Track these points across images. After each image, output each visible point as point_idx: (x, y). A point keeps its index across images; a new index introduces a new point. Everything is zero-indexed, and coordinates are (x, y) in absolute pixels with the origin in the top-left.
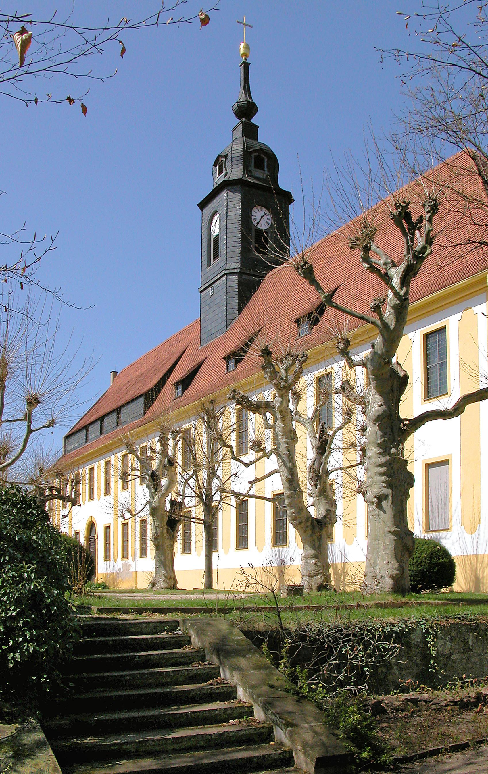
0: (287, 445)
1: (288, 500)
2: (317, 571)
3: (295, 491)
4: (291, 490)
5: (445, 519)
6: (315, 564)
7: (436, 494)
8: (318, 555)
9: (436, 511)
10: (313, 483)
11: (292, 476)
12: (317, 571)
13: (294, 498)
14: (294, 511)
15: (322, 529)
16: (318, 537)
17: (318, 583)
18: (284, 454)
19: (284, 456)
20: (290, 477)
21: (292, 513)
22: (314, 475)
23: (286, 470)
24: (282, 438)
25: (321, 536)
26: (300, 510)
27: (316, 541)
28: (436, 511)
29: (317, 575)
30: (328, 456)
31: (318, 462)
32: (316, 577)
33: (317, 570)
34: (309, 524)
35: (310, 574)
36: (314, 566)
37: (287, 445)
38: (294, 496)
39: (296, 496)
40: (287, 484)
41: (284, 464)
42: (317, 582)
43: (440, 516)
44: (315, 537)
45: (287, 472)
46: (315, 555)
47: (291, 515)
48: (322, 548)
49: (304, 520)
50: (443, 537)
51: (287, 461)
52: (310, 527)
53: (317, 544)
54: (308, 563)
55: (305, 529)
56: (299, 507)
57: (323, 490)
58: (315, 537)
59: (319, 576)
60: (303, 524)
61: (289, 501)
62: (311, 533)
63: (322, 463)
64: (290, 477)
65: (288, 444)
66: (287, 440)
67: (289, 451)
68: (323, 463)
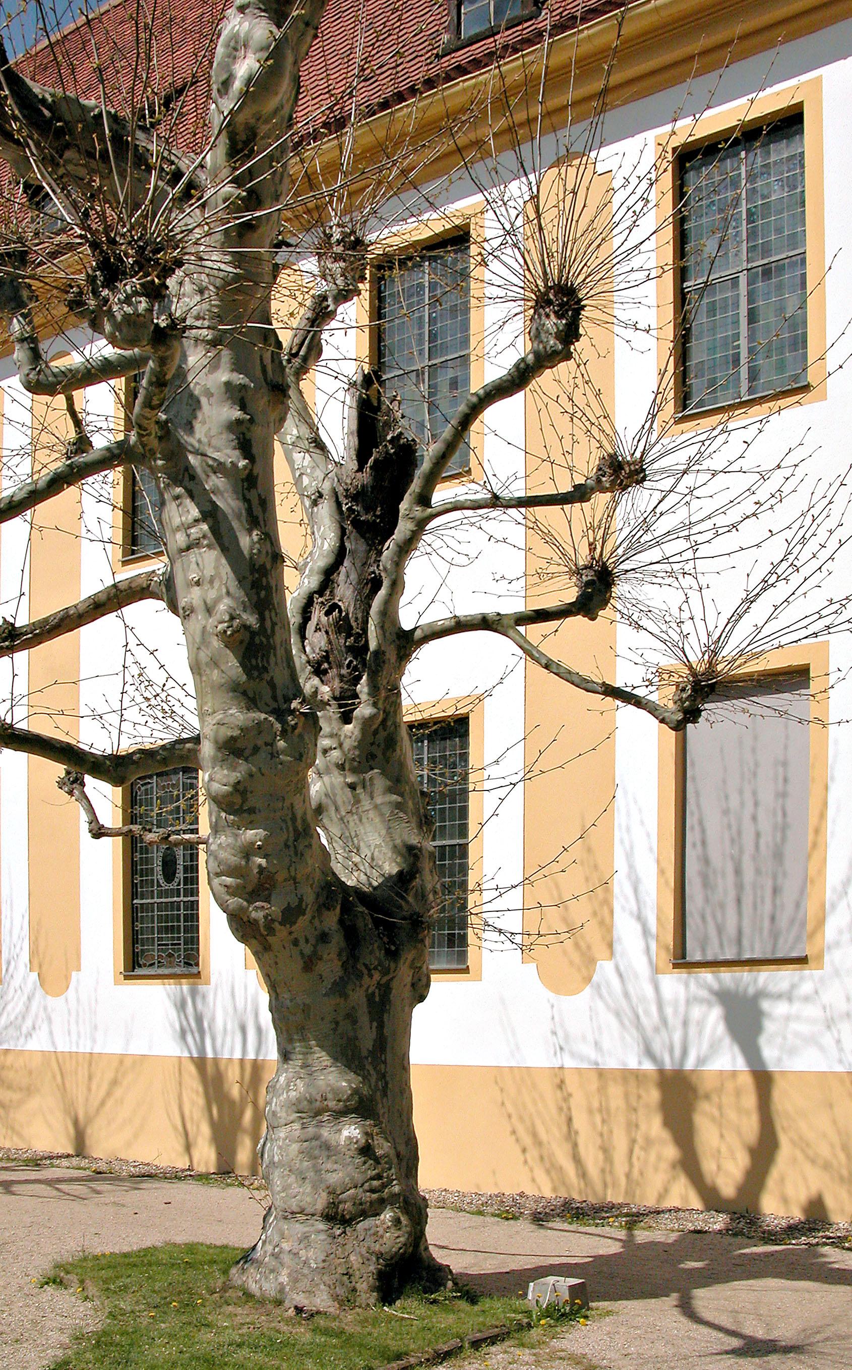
0: (237, 414)
1: (233, 768)
2: (372, 1191)
3: (281, 714)
4: (251, 700)
5: (773, 919)
6: (366, 1151)
7: (726, 812)
8: (372, 1099)
9: (726, 885)
10: (325, 689)
11: (262, 619)
12: (372, 1191)
13: (274, 755)
14: (265, 840)
15: (393, 955)
16: (370, 998)
17: (379, 1255)
18: (219, 468)
19: (216, 482)
20: (251, 619)
21: (248, 852)
22: (341, 641)
23: (226, 569)
24: (214, 365)
25: (385, 989)
26: (298, 835)
27: (364, 1018)
28: (726, 885)
29: (371, 1210)
30: (407, 548)
31: (353, 576)
32: (369, 1222)
33: (375, 1183)
34: (331, 920)
35: (333, 1205)
36: (359, 1160)
37: (237, 414)
38: (271, 744)
39: (281, 744)
40: (232, 665)
41: (215, 530)
42: (377, 1247)
43: (747, 900)
44: (358, 997)
45: (233, 584)
46: (361, 1100)
47: (234, 860)
48: (389, 1056)
49: (310, 897)
50: (772, 988)
51: (238, 517)
52: (337, 940)
53: (367, 1038)
54: (327, 1147)
55: (308, 950)
56: (294, 819)
57: (382, 735)
58: (358, 997)
59: (387, 1215)
60: (303, 921)
61: (235, 776)
62: (338, 972)
63: (376, 584)
64: (251, 619)
65: (243, 407)
66: (239, 379)
67: (245, 446)
68: (386, 583)
